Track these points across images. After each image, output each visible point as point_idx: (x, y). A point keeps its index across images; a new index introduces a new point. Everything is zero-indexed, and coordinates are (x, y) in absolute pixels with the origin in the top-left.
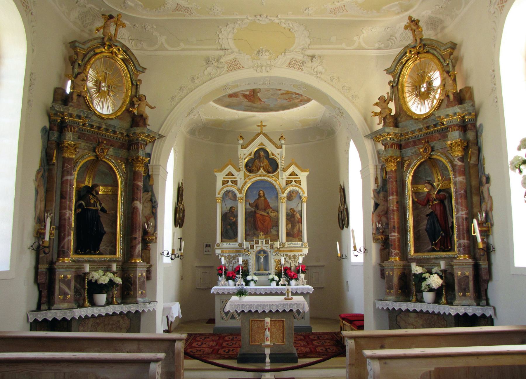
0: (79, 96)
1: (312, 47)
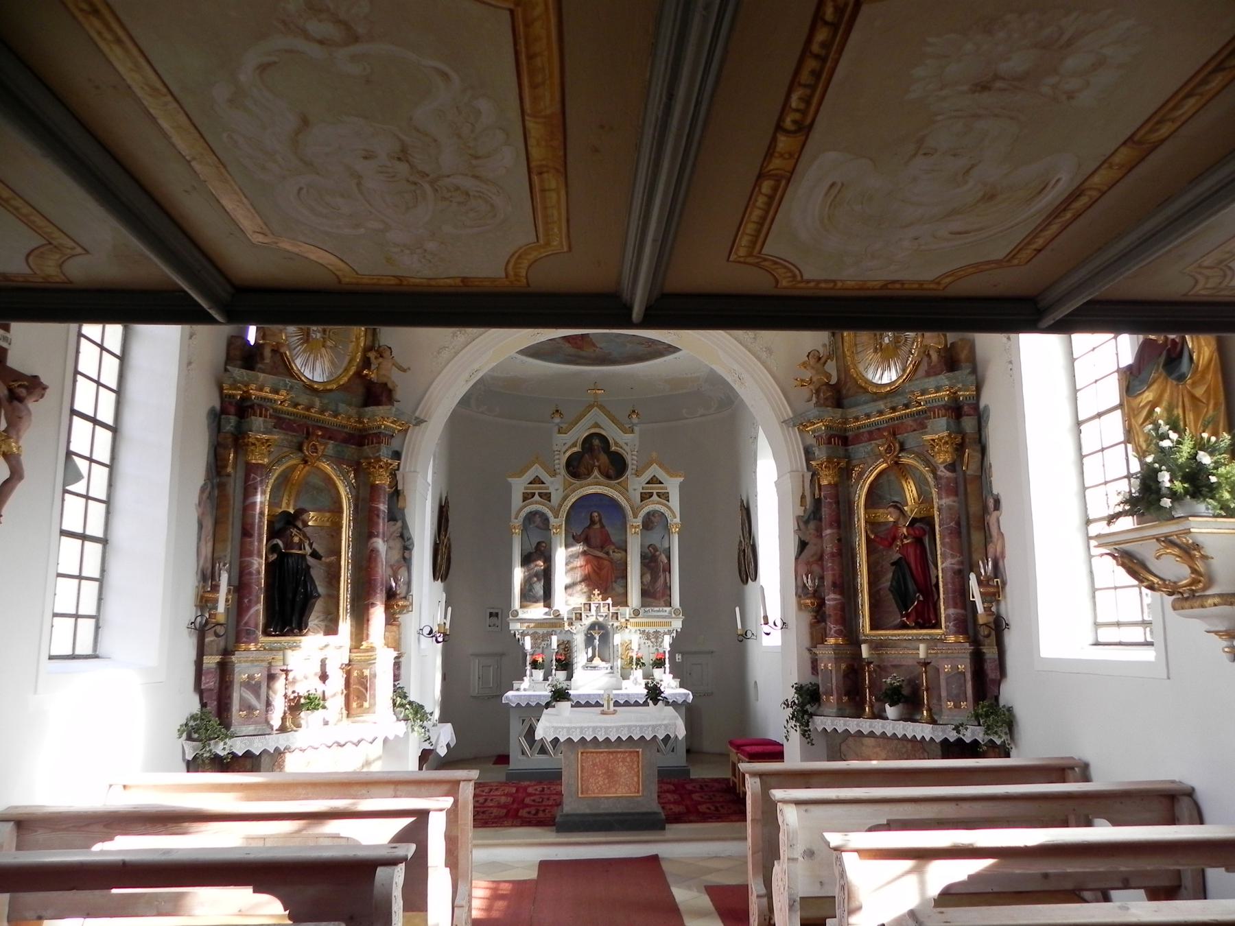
0: (275, 351)
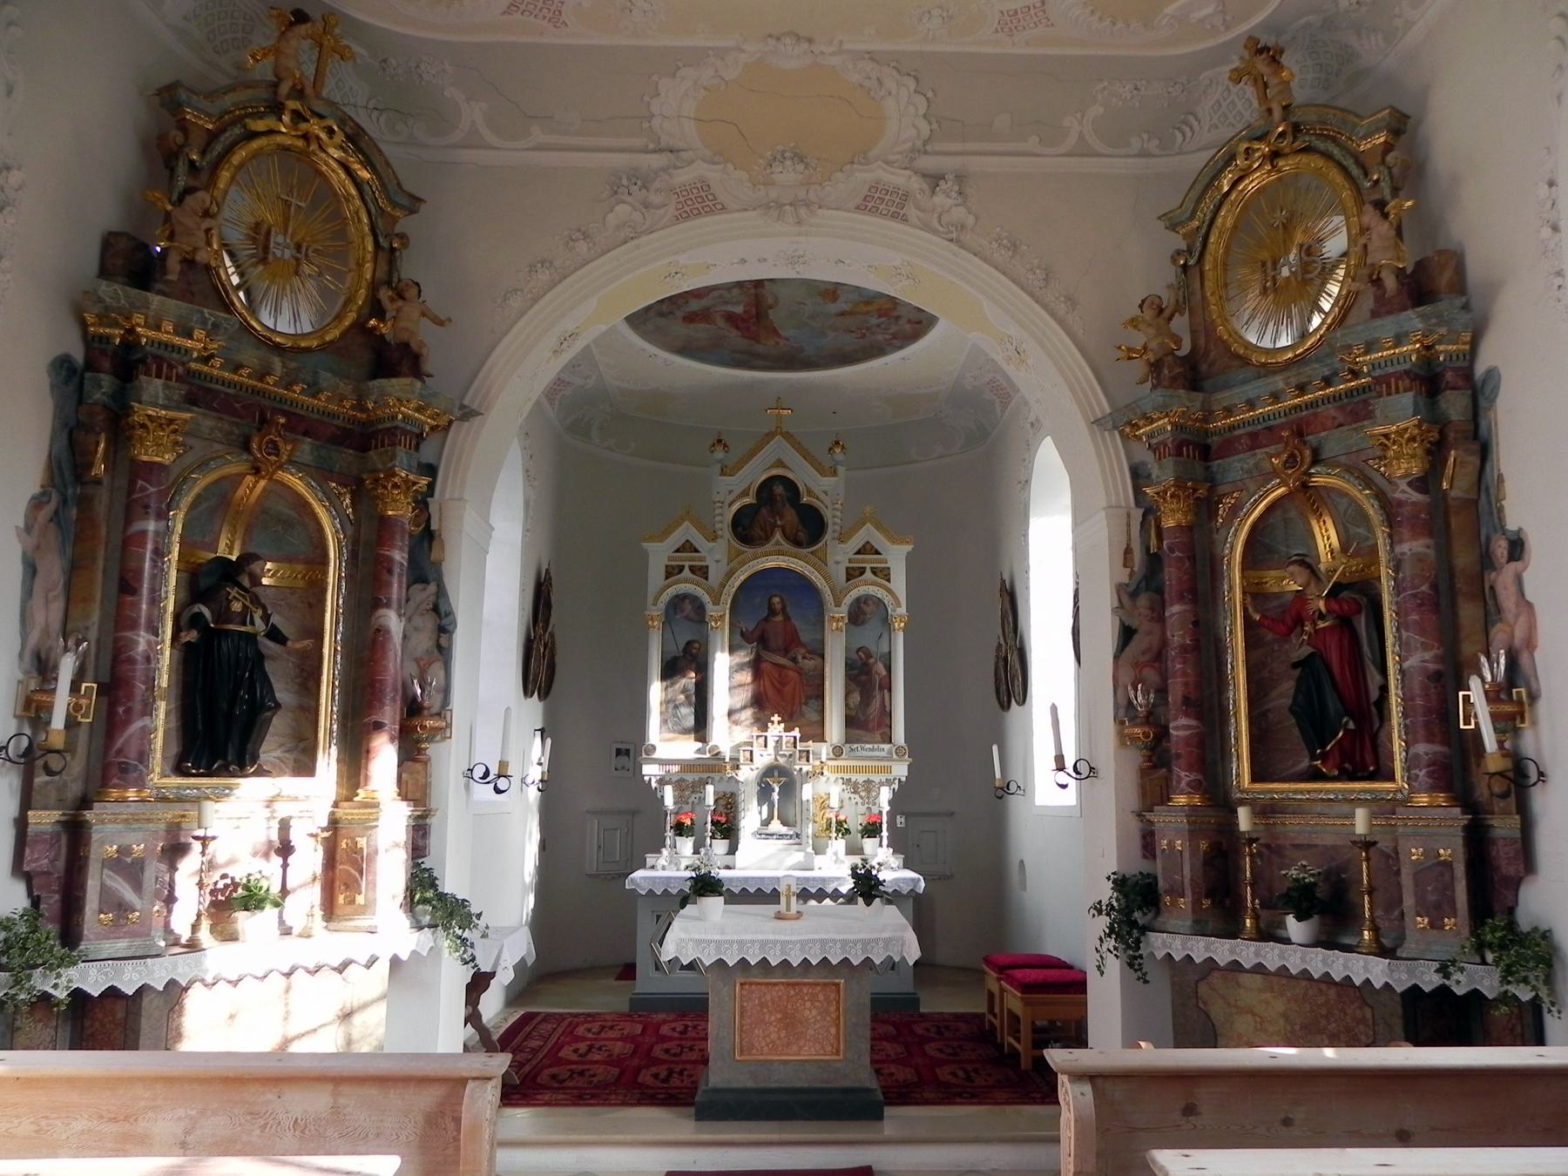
1: (938, 147)
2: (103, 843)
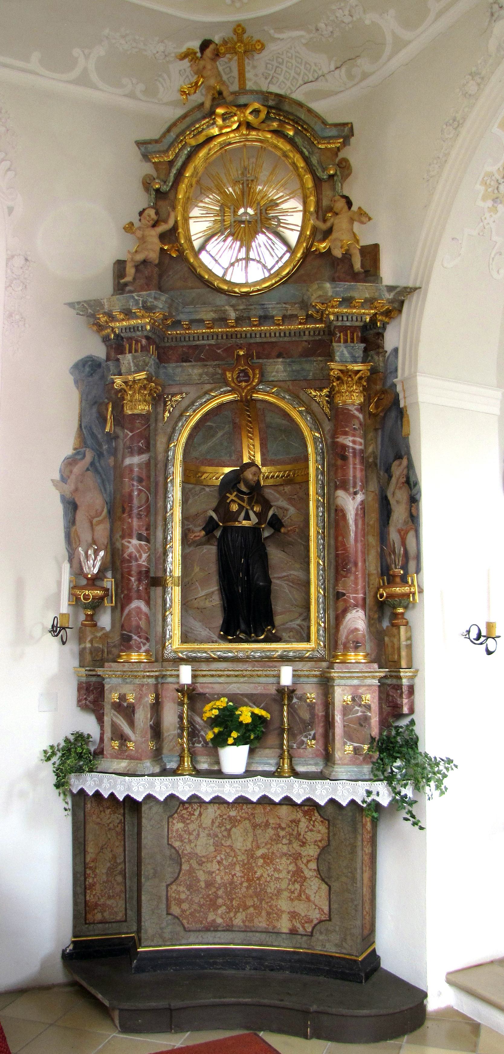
2: (111, 692)
